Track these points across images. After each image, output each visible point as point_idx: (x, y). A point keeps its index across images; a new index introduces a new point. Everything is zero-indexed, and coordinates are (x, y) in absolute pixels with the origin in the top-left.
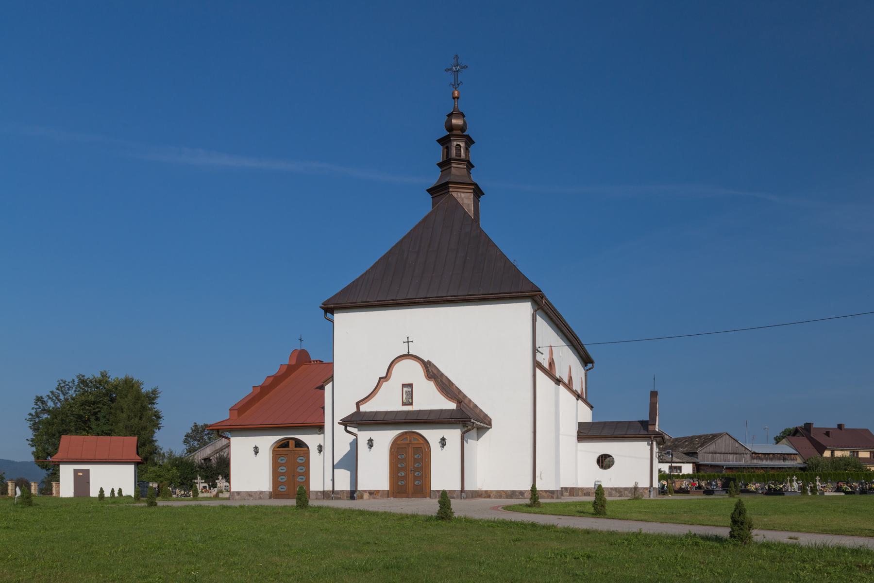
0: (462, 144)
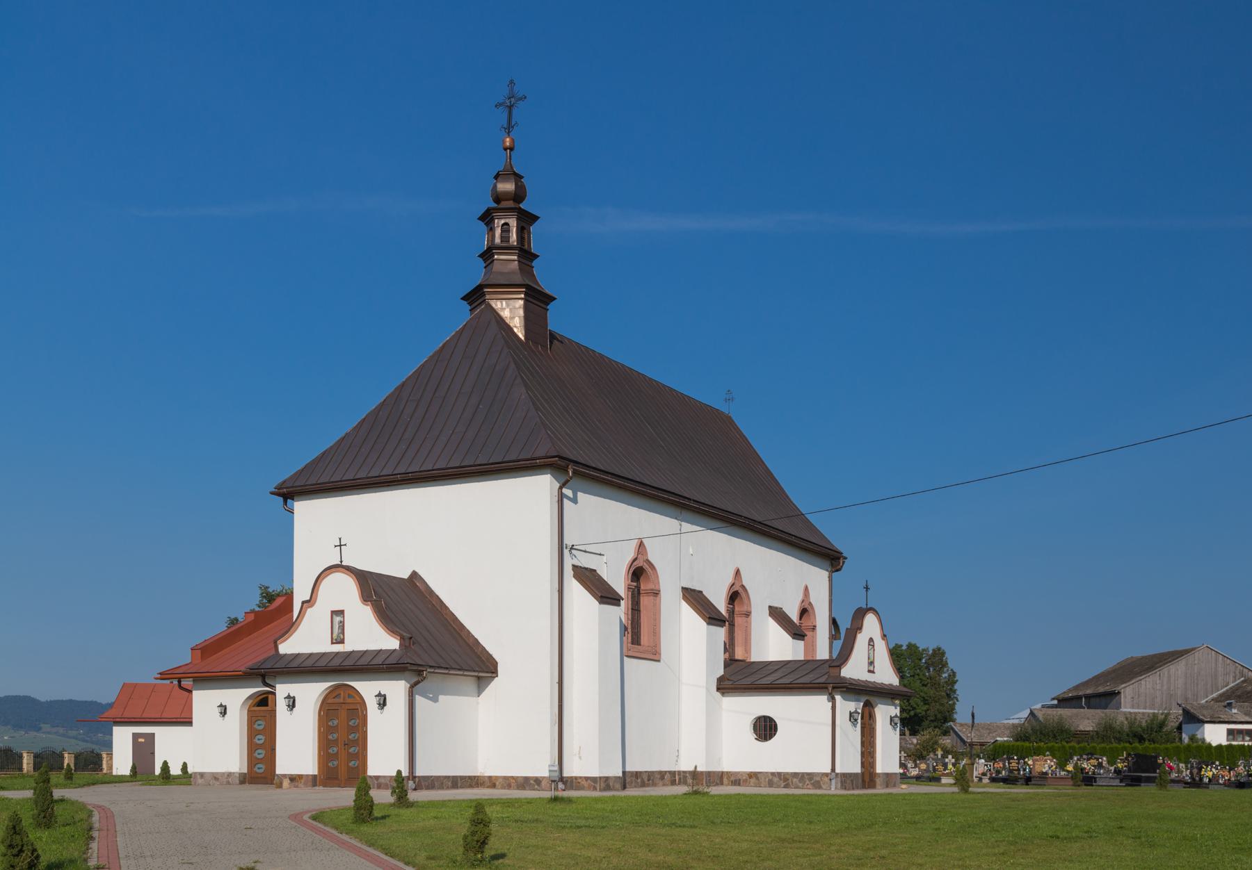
0: (513, 223)
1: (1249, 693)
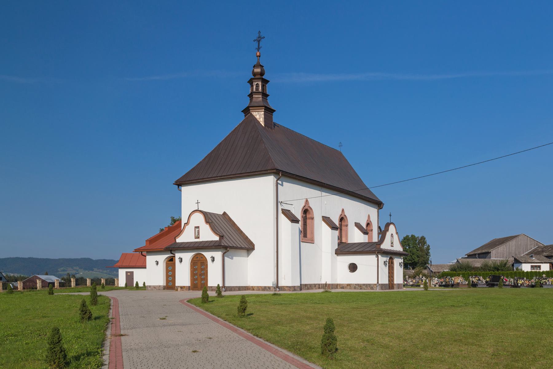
0: (260, 83)
1: (539, 251)
